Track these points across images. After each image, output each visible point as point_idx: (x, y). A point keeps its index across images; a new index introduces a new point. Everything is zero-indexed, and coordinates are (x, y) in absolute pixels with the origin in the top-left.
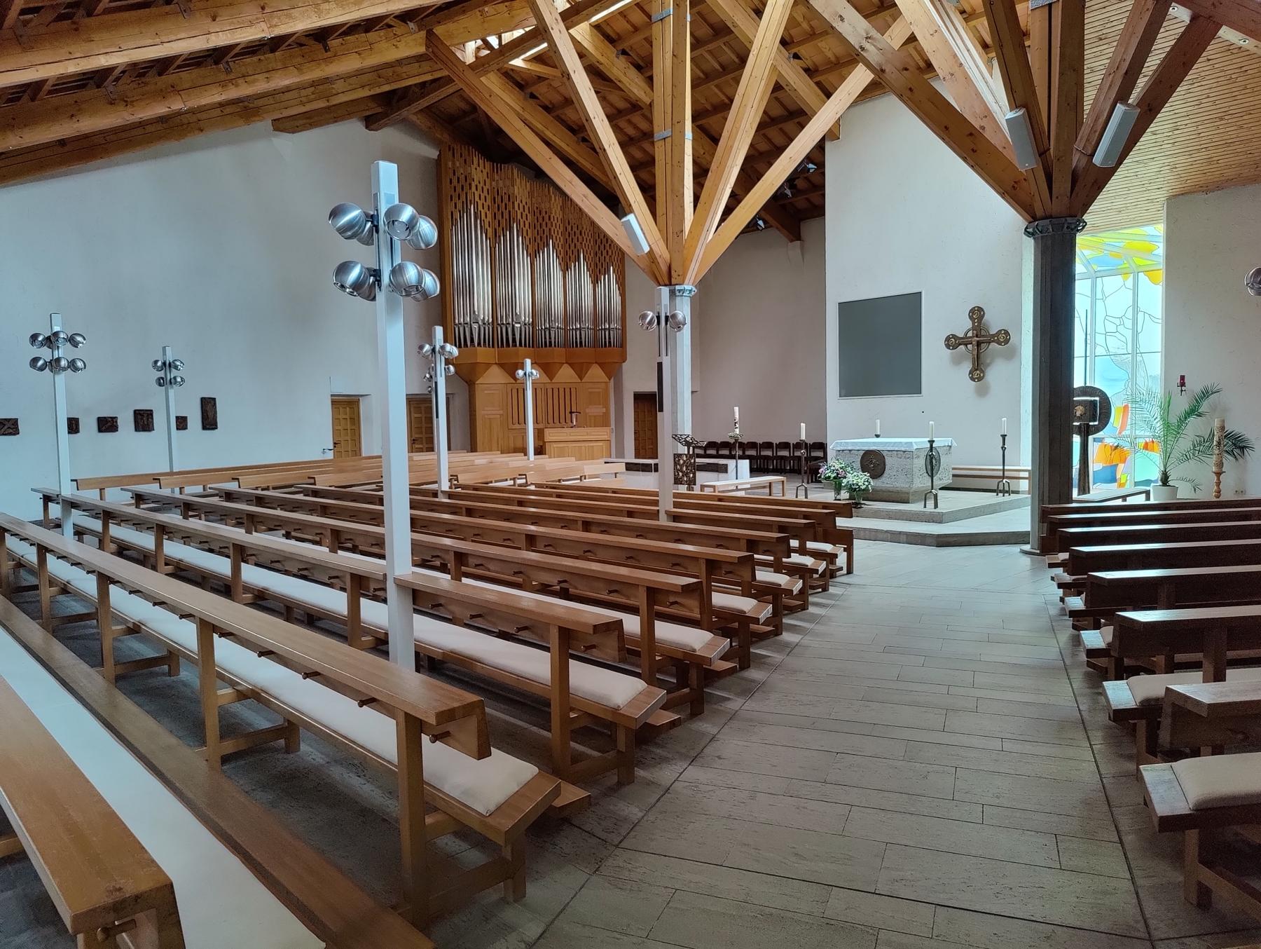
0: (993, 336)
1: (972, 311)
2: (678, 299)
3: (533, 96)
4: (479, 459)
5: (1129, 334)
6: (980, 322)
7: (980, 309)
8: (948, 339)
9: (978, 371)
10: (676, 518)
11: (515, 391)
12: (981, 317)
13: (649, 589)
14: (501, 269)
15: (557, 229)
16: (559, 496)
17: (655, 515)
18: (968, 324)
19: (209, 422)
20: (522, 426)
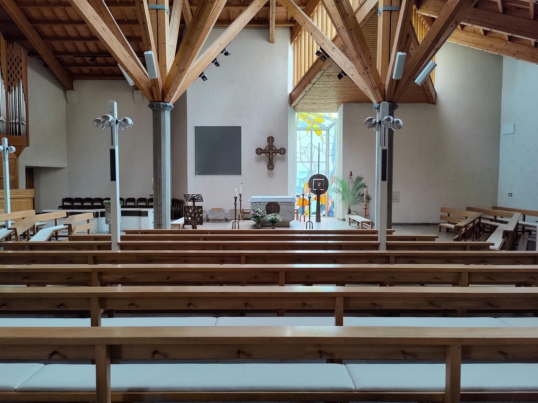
0: (278, 150)
1: (269, 138)
5: (309, 154)
7: (272, 138)
8: (257, 150)
9: (271, 166)
13: (344, 298)
16: (205, 239)
17: (109, 247)
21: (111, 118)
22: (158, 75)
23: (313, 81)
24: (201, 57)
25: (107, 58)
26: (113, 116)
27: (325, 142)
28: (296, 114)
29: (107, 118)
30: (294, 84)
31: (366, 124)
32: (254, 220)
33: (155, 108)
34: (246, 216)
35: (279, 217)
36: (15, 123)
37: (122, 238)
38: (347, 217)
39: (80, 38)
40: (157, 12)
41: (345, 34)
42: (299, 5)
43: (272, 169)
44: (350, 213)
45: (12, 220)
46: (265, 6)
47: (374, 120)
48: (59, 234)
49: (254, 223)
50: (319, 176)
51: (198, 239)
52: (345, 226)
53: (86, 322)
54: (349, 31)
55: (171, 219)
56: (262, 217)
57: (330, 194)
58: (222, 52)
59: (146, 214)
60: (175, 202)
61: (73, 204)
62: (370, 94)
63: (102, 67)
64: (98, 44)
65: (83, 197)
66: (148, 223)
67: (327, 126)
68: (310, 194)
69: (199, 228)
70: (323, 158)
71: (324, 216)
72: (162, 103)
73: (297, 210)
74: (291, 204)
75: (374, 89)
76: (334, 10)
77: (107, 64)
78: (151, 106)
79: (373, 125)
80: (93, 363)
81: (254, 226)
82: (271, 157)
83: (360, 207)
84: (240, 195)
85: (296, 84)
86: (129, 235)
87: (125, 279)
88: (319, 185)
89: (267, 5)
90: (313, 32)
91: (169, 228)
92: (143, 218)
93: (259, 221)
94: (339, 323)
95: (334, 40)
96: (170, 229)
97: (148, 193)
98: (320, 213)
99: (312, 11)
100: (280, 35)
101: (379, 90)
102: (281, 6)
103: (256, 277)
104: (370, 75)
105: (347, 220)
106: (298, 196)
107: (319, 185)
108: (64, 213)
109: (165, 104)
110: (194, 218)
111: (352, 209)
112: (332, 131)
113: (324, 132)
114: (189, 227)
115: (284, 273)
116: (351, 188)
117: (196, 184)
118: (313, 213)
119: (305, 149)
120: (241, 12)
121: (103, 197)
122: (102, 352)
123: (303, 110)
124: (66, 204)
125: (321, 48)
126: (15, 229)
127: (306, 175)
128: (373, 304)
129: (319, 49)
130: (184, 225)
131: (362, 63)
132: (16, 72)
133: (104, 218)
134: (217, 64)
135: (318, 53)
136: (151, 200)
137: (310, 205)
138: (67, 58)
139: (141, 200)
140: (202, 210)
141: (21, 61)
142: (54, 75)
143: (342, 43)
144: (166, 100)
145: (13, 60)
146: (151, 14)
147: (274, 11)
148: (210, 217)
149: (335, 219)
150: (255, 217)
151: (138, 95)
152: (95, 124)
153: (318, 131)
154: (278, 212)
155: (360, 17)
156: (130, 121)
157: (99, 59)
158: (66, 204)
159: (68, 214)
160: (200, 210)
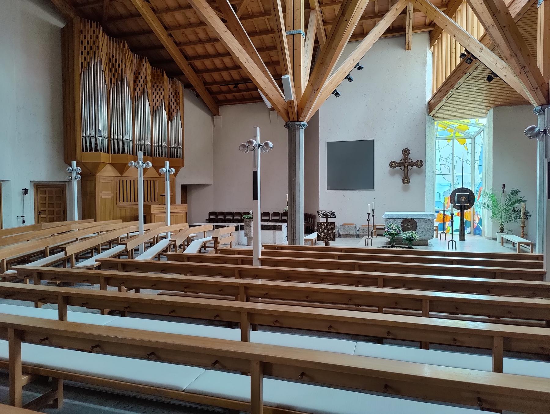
0: (415, 163)
1: (404, 150)
3: (171, 35)
4: (99, 225)
6: (408, 156)
7: (408, 150)
8: (391, 163)
9: (406, 180)
11: (121, 182)
12: (409, 153)
14: (115, 110)
15: (149, 89)
16: (340, 257)
17: (250, 262)
20: (136, 203)
21: (255, 142)
22: (293, 97)
23: (456, 86)
24: (335, 74)
25: (248, 84)
26: (256, 141)
27: (470, 151)
28: (436, 123)
29: (251, 143)
30: (433, 91)
31: (526, 134)
32: (388, 237)
33: (291, 128)
34: (379, 232)
35: (416, 235)
36: (174, 147)
37: (263, 253)
38: (499, 236)
39: (226, 68)
40: (294, 37)
41: (496, 33)
42: (439, 7)
43: (408, 183)
44: (502, 231)
45: (171, 232)
46: (401, 14)
47: (537, 129)
48: (207, 245)
49: (389, 240)
50: (463, 190)
51: (333, 257)
52: (497, 249)
53: (235, 334)
54: (502, 28)
55: (304, 234)
56: (397, 234)
57: (476, 210)
58: (355, 67)
59: (280, 228)
60: (308, 217)
61: (218, 218)
62: (528, 95)
63: (244, 92)
64: (241, 72)
65: (225, 211)
66: (281, 238)
67: (473, 134)
68: (452, 210)
69: (332, 244)
70: (468, 169)
71: (469, 233)
72: (297, 123)
73: (437, 227)
74: (430, 220)
75: (533, 90)
76: (482, 8)
77: (248, 89)
78: (287, 126)
79: (533, 134)
80: (244, 373)
81: (389, 244)
82: (406, 170)
83: (517, 225)
84: (373, 210)
85: (435, 91)
86: (269, 250)
87: (268, 294)
88: (463, 200)
89: (404, 12)
90: (457, 33)
91: (302, 244)
92: (278, 232)
93: (394, 240)
94: (498, 368)
95: (481, 40)
96: (303, 246)
97: (282, 207)
98: (464, 230)
99: (455, 11)
100: (417, 41)
101: (541, 91)
102: (418, 11)
103: (396, 303)
104: (529, 74)
105: (499, 240)
106: (437, 212)
107: (463, 200)
108: (211, 225)
109: (299, 123)
110: (327, 234)
111: (505, 227)
112: (479, 140)
113: (469, 141)
114: (322, 244)
115: (428, 301)
116: (504, 202)
117: (328, 200)
118: (456, 231)
119: (445, 160)
120: (375, 24)
121: (242, 211)
122: (256, 367)
123: (443, 118)
124: (211, 217)
125: (466, 50)
126: (175, 241)
127: (447, 188)
128: (542, 348)
129: (463, 51)
130: (315, 240)
131: (518, 62)
132: (175, 104)
133: (243, 232)
134: (350, 80)
135: (462, 55)
136: (285, 214)
137: (452, 222)
138: (214, 88)
139: (276, 214)
140: (335, 227)
141: (179, 94)
142: (202, 101)
143: (491, 42)
144: (301, 119)
145: (173, 94)
146: (288, 39)
147: (411, 17)
148: (341, 233)
149: (484, 239)
150: (389, 234)
151: (274, 114)
152: (241, 148)
153: (462, 140)
154: (415, 230)
155: (514, 11)
156: (271, 144)
157: (241, 86)
158: (211, 217)
159: (215, 227)
160: (333, 226)
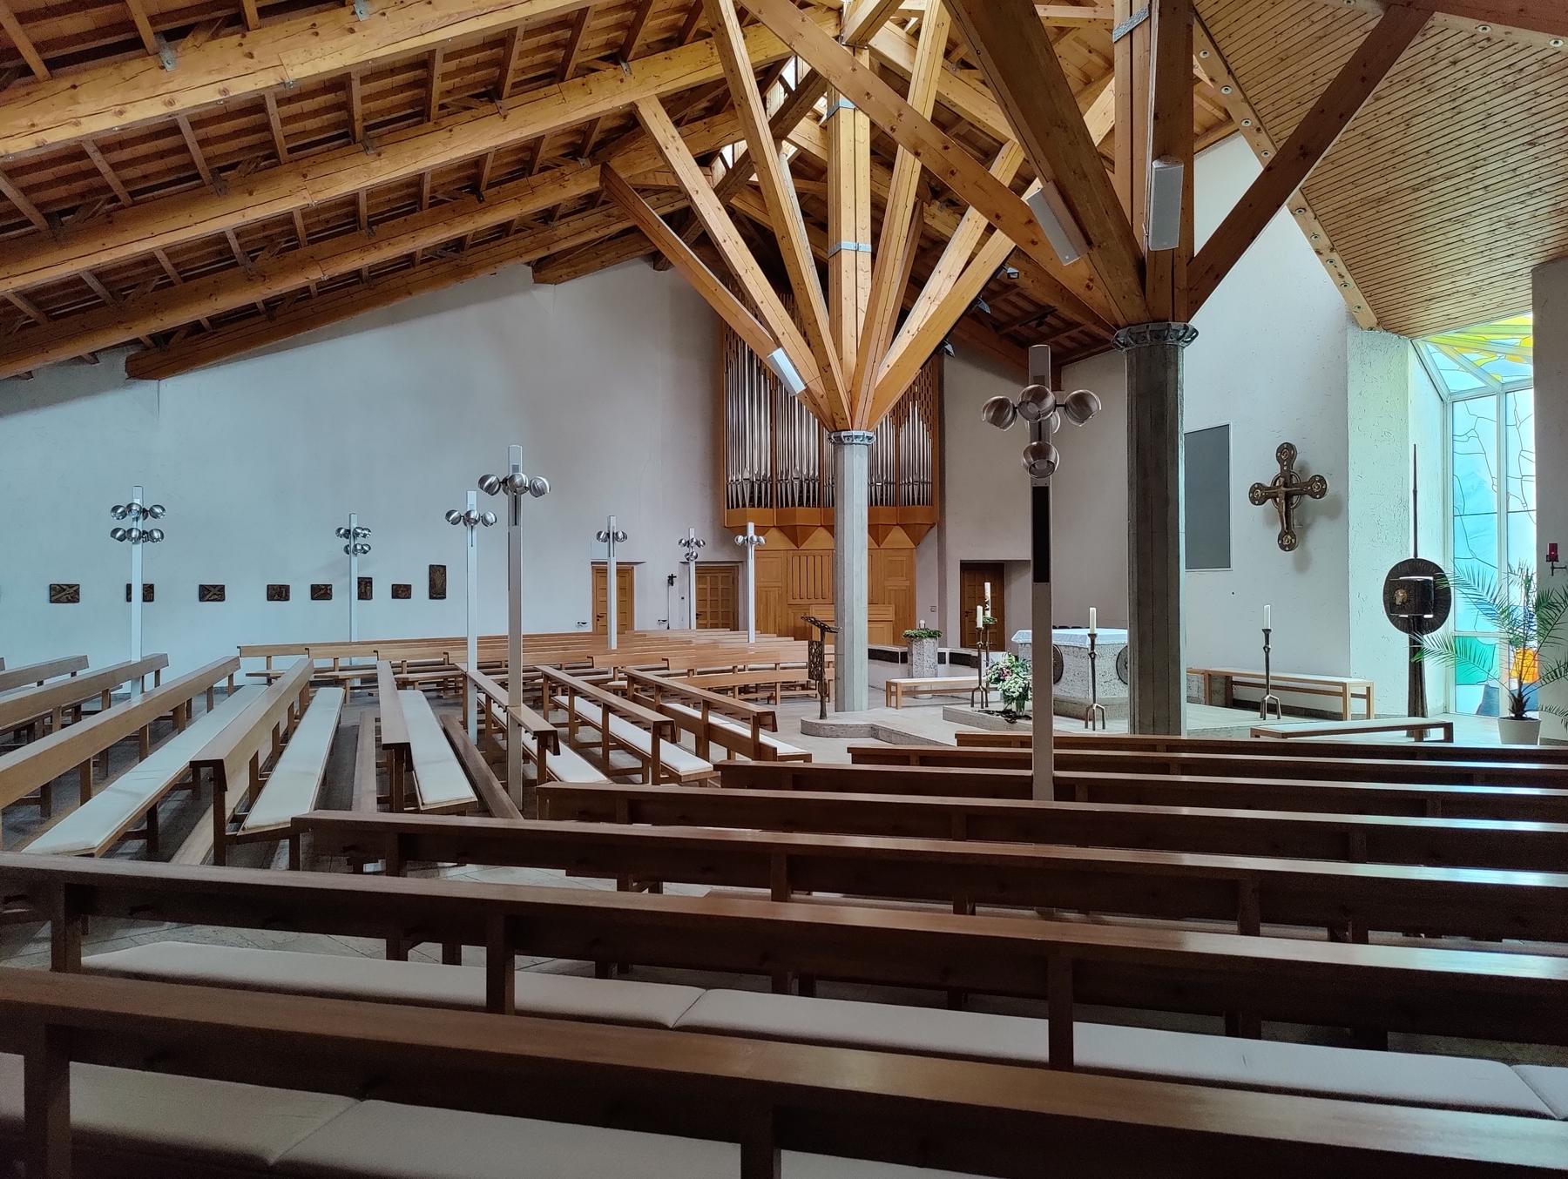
0: (1306, 484)
1: (1281, 450)
2: (847, 449)
8: (1253, 490)
9: (1289, 538)
10: (1064, 790)
12: (1292, 458)
18: (1276, 469)
19: (437, 590)
